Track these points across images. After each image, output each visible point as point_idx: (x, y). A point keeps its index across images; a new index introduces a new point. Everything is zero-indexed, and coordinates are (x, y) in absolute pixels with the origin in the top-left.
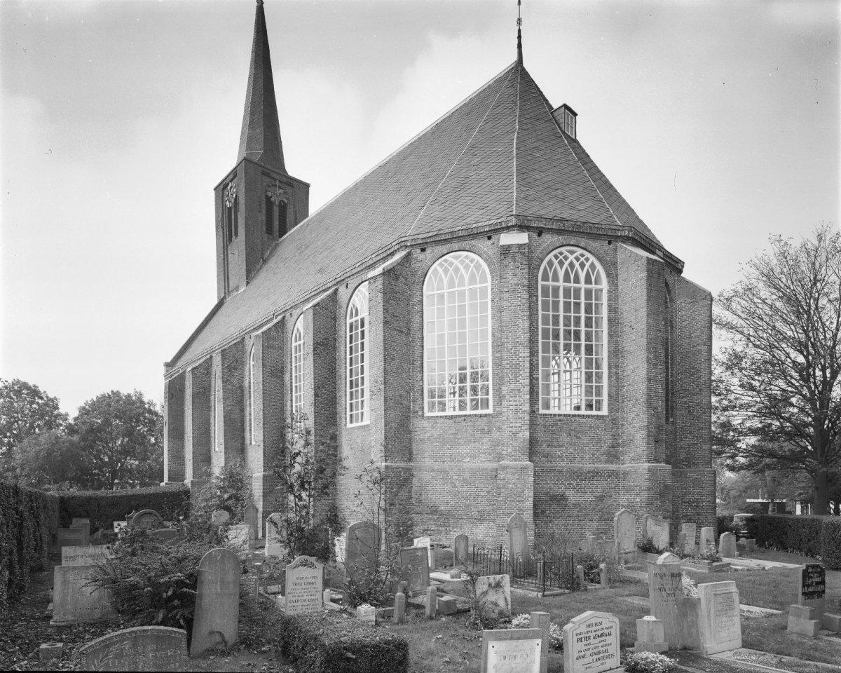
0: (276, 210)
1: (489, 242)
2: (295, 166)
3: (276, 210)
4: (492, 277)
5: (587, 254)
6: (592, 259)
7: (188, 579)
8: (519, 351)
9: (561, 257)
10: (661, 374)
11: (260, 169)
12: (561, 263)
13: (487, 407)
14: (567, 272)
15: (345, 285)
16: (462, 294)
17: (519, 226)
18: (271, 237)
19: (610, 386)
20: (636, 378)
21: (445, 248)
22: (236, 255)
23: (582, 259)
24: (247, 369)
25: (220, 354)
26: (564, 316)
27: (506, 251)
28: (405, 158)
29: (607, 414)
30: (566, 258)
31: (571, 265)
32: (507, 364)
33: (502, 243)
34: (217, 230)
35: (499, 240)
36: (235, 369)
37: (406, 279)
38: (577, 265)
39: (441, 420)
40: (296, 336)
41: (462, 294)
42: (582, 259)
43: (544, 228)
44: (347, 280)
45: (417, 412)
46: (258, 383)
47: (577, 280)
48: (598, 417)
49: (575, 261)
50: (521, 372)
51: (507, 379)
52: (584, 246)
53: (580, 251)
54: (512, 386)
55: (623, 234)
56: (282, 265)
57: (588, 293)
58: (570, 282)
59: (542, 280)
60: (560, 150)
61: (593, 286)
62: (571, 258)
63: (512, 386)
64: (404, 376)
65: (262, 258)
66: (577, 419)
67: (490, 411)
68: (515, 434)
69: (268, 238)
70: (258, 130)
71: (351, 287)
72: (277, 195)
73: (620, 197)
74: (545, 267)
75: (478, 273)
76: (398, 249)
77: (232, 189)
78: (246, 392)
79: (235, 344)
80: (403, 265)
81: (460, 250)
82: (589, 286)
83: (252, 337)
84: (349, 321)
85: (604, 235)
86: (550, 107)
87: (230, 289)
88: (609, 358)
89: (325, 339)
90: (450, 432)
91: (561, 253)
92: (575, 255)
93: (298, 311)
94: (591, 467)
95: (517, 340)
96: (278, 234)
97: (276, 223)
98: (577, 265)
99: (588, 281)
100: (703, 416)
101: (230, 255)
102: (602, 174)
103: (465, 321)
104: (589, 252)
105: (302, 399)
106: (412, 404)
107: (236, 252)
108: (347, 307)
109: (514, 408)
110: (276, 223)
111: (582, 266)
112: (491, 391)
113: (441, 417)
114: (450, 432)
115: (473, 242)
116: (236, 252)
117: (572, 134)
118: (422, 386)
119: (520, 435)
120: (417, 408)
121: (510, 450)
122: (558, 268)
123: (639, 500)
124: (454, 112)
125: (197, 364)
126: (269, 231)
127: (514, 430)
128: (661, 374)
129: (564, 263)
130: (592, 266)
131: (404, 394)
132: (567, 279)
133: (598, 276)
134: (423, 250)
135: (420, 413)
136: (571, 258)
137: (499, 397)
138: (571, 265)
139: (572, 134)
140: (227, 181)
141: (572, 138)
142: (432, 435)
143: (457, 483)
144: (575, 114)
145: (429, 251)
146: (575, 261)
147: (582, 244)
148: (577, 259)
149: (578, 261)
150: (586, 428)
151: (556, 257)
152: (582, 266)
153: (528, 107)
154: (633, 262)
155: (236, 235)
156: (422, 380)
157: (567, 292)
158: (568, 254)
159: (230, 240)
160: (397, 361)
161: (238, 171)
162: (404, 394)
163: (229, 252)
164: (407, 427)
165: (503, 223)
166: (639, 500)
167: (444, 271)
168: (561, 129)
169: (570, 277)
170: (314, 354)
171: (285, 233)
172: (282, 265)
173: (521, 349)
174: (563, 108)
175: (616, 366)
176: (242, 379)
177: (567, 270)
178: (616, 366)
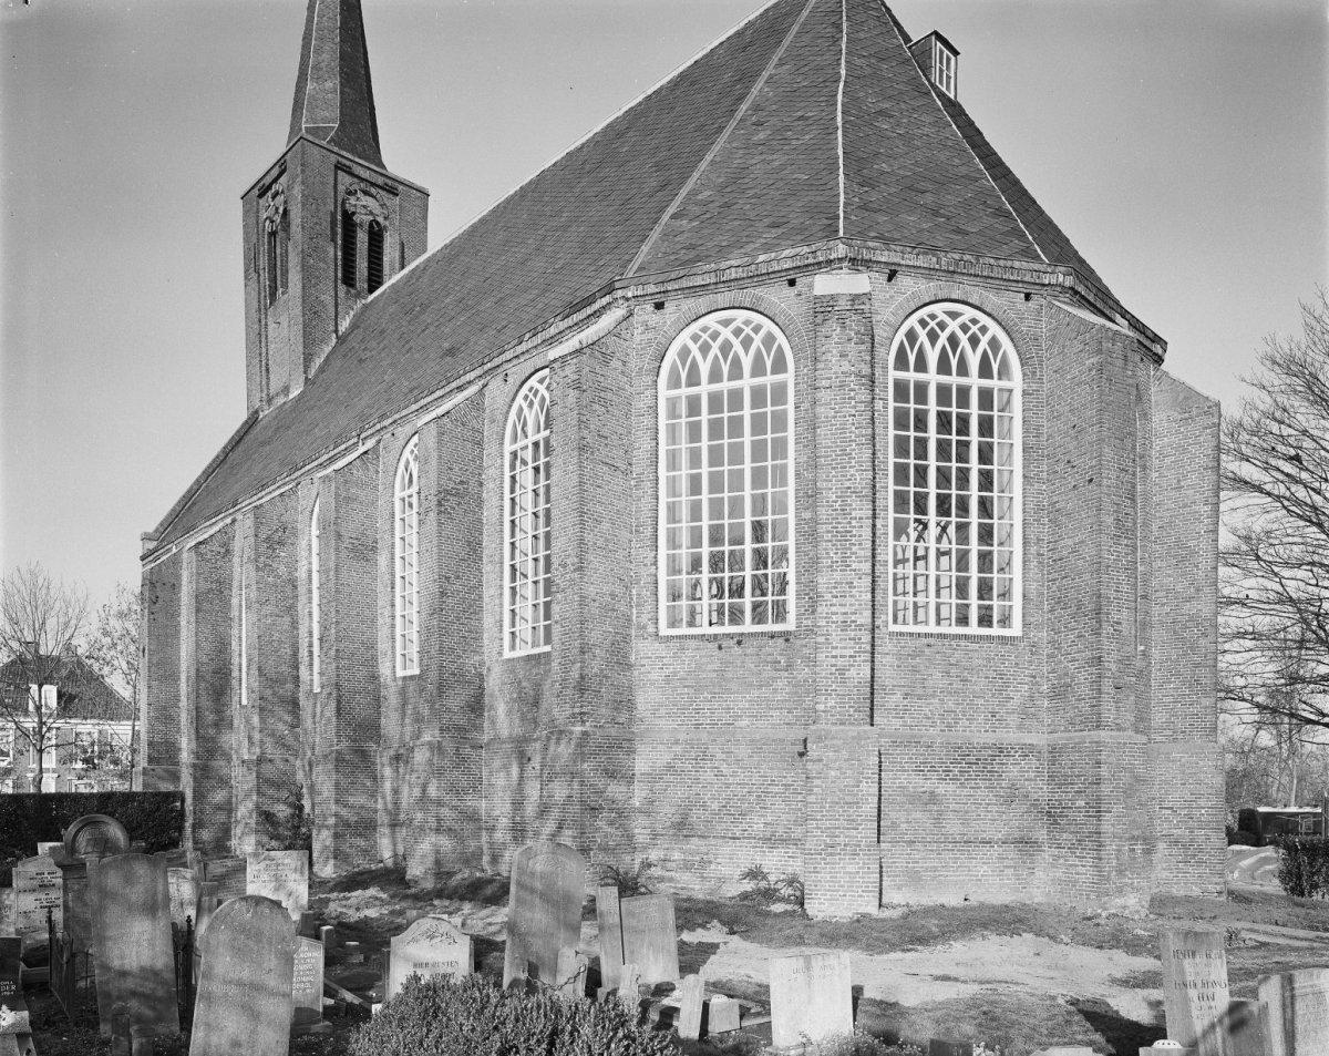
0: (362, 238)
1: (793, 291)
2: (399, 155)
3: (362, 238)
4: (797, 362)
5: (984, 320)
6: (994, 329)
7: (310, 909)
8: (851, 505)
9: (933, 324)
10: (1127, 554)
11: (333, 158)
12: (933, 337)
13: (784, 620)
14: (759, 359)
15: (502, 376)
16: (736, 398)
17: (853, 260)
18: (353, 291)
19: (1025, 579)
20: (1080, 563)
21: (703, 303)
22: (285, 324)
23: (974, 329)
24: (304, 543)
25: (251, 515)
26: (938, 441)
27: (823, 308)
28: (620, 135)
29: (1020, 634)
30: (942, 326)
31: (953, 340)
32: (828, 532)
33: (817, 292)
34: (246, 278)
35: (811, 286)
36: (281, 543)
37: (624, 363)
38: (964, 340)
39: (693, 644)
40: (403, 478)
41: (736, 398)
42: (974, 329)
43: (900, 265)
44: (506, 366)
45: (644, 627)
46: (327, 572)
47: (921, 365)
48: (1003, 640)
49: (960, 333)
50: (854, 549)
51: (826, 562)
52: (977, 303)
53: (969, 313)
54: (837, 576)
55: (1053, 281)
56: (374, 344)
57: (986, 398)
58: (907, 370)
59: (896, 369)
60: (928, 119)
61: (994, 383)
62: (953, 326)
63: (837, 576)
64: (620, 554)
65: (336, 331)
66: (963, 643)
67: (790, 625)
68: (842, 671)
69: (348, 292)
70: (329, 85)
71: (513, 380)
72: (366, 207)
73: (1041, 212)
74: (902, 343)
75: (769, 356)
76: (609, 304)
77: (294, 189)
78: (302, 590)
79: (281, 495)
80: (618, 336)
81: (734, 308)
82: (986, 383)
83: (315, 480)
84: (508, 448)
85: (1017, 282)
86: (907, 39)
87: (272, 392)
88: (1025, 524)
89: (462, 482)
90: (710, 667)
91: (933, 317)
92: (960, 320)
93: (408, 429)
94: (990, 738)
95: (848, 484)
96: (366, 286)
97: (362, 265)
98: (964, 340)
99: (985, 370)
100: (1203, 642)
101: (271, 326)
102: (1007, 168)
103: (767, 445)
104: (989, 315)
105: (1255, 462)
106: (634, 611)
107: (284, 320)
108: (506, 420)
109: (841, 618)
110: (362, 265)
111: (974, 341)
112: (792, 589)
113: (693, 637)
114: (710, 667)
115: (758, 291)
116: (284, 320)
117: (948, 88)
118: (656, 576)
119: (853, 672)
120: (644, 619)
121: (831, 703)
122: (927, 345)
123: (1083, 803)
124: (716, 48)
125: (206, 536)
126: (349, 279)
127: (840, 662)
128: (1127, 554)
129: (938, 336)
130: (994, 343)
131: (619, 590)
132: (944, 367)
133: (780, 354)
134: (659, 306)
135: (651, 629)
136: (726, 333)
137: (811, 599)
138: (953, 340)
139: (948, 88)
140: (268, 180)
141: (949, 99)
142: (675, 674)
143: (724, 768)
144: (956, 53)
145: (670, 307)
146: (960, 333)
147: (974, 300)
148: (965, 328)
149: (965, 333)
150: (980, 662)
151: (923, 323)
152: (974, 341)
153: (862, 35)
154: (1074, 335)
155: (285, 285)
156: (655, 563)
157: (943, 393)
158: (947, 319)
159: (273, 295)
160: (605, 526)
161: (288, 161)
162: (619, 590)
163: (270, 319)
164: (625, 657)
165: (819, 253)
166: (1083, 803)
167: (700, 349)
168: (929, 81)
169: (908, 360)
170: (440, 513)
171: (380, 284)
172: (374, 344)
173: (854, 502)
174: (933, 37)
175: (1038, 540)
176: (293, 565)
177: (985, 354)
178: (1038, 540)
